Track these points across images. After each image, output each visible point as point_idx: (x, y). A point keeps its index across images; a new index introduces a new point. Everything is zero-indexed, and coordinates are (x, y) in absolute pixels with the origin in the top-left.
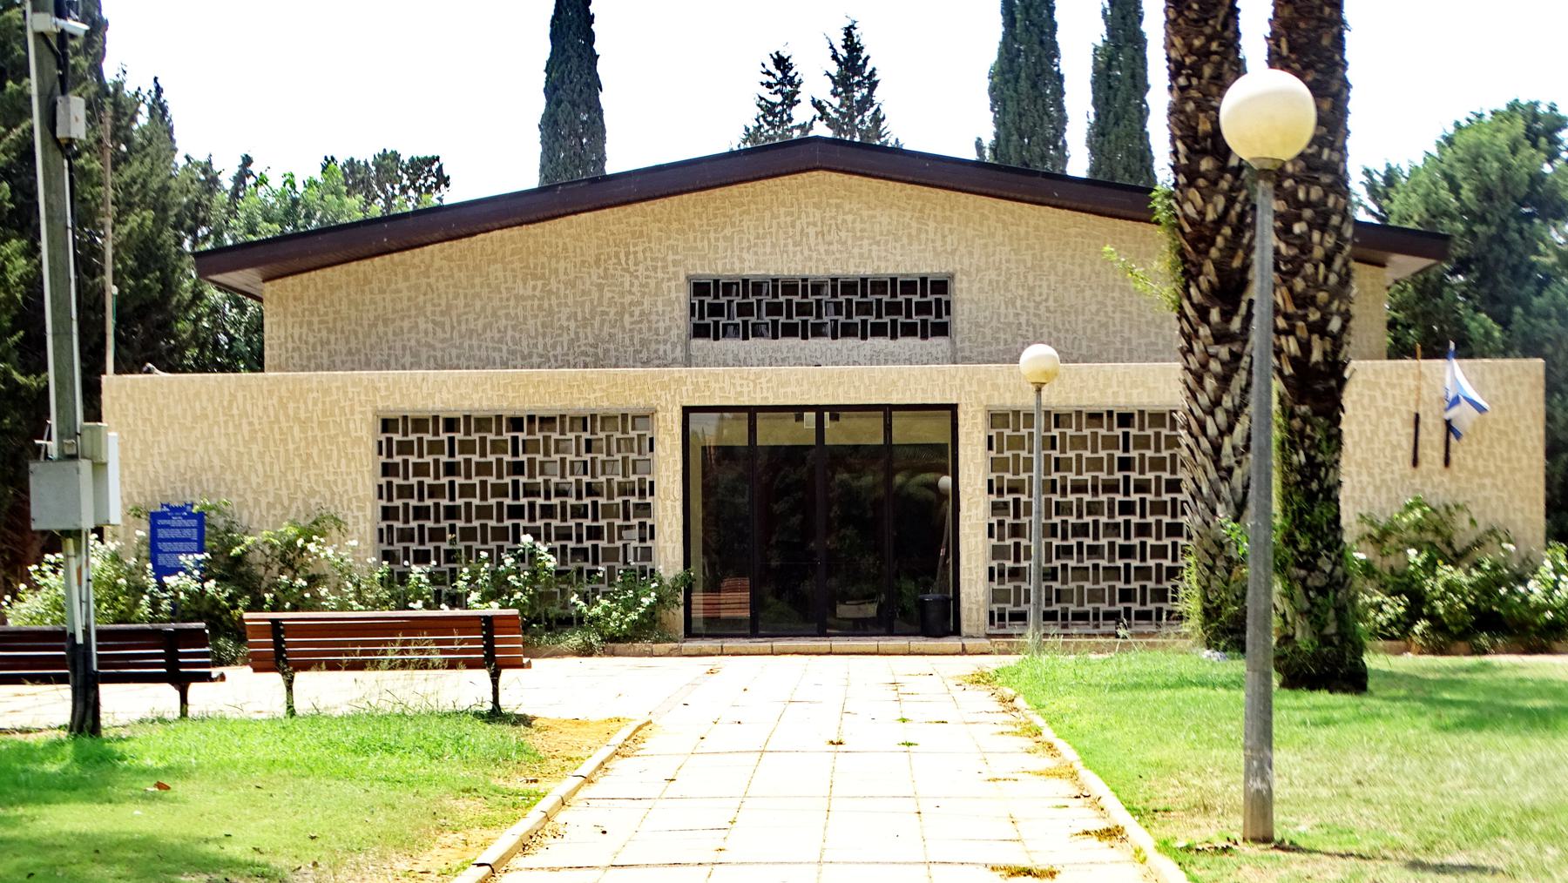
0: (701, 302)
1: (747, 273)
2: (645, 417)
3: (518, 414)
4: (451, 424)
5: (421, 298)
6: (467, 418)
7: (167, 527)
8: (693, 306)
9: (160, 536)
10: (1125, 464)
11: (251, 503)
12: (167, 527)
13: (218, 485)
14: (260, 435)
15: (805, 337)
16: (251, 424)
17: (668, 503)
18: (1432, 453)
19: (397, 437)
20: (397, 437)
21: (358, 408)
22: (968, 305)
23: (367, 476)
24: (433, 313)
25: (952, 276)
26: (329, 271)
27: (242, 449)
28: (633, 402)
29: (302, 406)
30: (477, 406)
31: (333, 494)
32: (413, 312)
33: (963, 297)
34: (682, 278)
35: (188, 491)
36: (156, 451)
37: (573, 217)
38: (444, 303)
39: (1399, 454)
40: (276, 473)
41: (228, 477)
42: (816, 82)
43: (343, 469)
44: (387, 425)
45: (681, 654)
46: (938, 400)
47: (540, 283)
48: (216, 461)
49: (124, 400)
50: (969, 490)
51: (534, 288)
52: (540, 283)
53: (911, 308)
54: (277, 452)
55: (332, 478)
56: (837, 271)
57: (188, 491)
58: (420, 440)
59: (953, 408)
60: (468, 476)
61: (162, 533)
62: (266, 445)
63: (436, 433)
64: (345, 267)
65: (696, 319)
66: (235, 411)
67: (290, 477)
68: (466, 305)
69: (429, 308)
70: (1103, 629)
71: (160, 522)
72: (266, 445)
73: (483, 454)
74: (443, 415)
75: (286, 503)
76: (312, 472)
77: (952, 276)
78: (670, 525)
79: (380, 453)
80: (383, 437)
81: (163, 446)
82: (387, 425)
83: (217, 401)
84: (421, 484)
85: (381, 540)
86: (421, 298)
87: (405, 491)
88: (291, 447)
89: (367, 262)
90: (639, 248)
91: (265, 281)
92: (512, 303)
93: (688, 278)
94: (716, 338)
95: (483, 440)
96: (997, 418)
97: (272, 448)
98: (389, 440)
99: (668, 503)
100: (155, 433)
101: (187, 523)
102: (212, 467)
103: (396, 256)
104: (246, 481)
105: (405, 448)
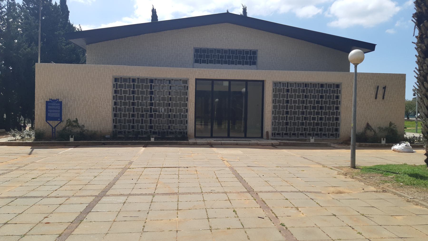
0: (197, 54)
1: (208, 47)
2: (186, 81)
3: (152, 78)
4: (134, 80)
6: (138, 79)
7: (51, 105)
8: (195, 55)
10: (322, 97)
11: (77, 100)
12: (51, 105)
15: (222, 64)
17: (192, 103)
18: (380, 96)
19: (119, 83)
20: (119, 83)
22: (260, 59)
23: (110, 93)
25: (257, 50)
28: (183, 77)
30: (141, 76)
33: (260, 55)
34: (192, 48)
35: (59, 96)
39: (372, 96)
44: (116, 80)
46: (261, 79)
50: (268, 102)
53: (248, 58)
56: (230, 48)
57: (59, 96)
58: (125, 84)
59: (263, 82)
60: (138, 95)
63: (130, 83)
65: (195, 58)
70: (300, 138)
71: (49, 104)
73: (142, 89)
74: (131, 78)
75: (87, 100)
77: (257, 50)
78: (192, 109)
79: (114, 87)
80: (115, 83)
82: (116, 80)
84: (125, 96)
85: (114, 111)
87: (121, 98)
91: (87, 44)
93: (194, 48)
94: (200, 63)
95: (142, 85)
96: (275, 84)
98: (117, 84)
99: (192, 103)
101: (57, 104)
103: (120, 39)
105: (121, 86)
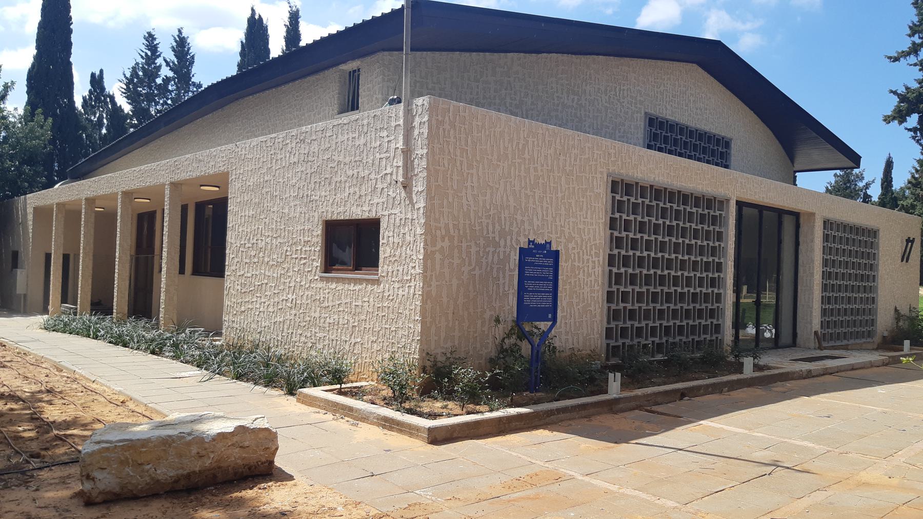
5: (503, 91)
9: (527, 274)
13: (511, 225)
14: (541, 181)
16: (536, 169)
21: (599, 169)
24: (511, 104)
26: (437, 54)
27: (528, 192)
29: (568, 159)
30: (657, 179)
31: (582, 241)
32: (497, 101)
36: (469, 184)
37: (595, 57)
38: (518, 98)
40: (550, 218)
41: (519, 217)
42: (167, 52)
43: (589, 220)
45: (120, 341)
47: (576, 98)
48: (512, 203)
49: (447, 126)
51: (573, 101)
52: (576, 98)
54: (551, 198)
55: (582, 227)
61: (529, 272)
62: (545, 192)
64: (451, 54)
66: (526, 156)
67: (558, 223)
68: (532, 103)
69: (508, 100)
71: (529, 259)
72: (545, 192)
76: (572, 219)
81: (475, 179)
83: (515, 144)
86: (503, 91)
88: (560, 195)
89: (468, 54)
90: (625, 88)
92: (560, 108)
97: (548, 195)
100: (470, 167)
102: (508, 206)
104: (531, 223)
